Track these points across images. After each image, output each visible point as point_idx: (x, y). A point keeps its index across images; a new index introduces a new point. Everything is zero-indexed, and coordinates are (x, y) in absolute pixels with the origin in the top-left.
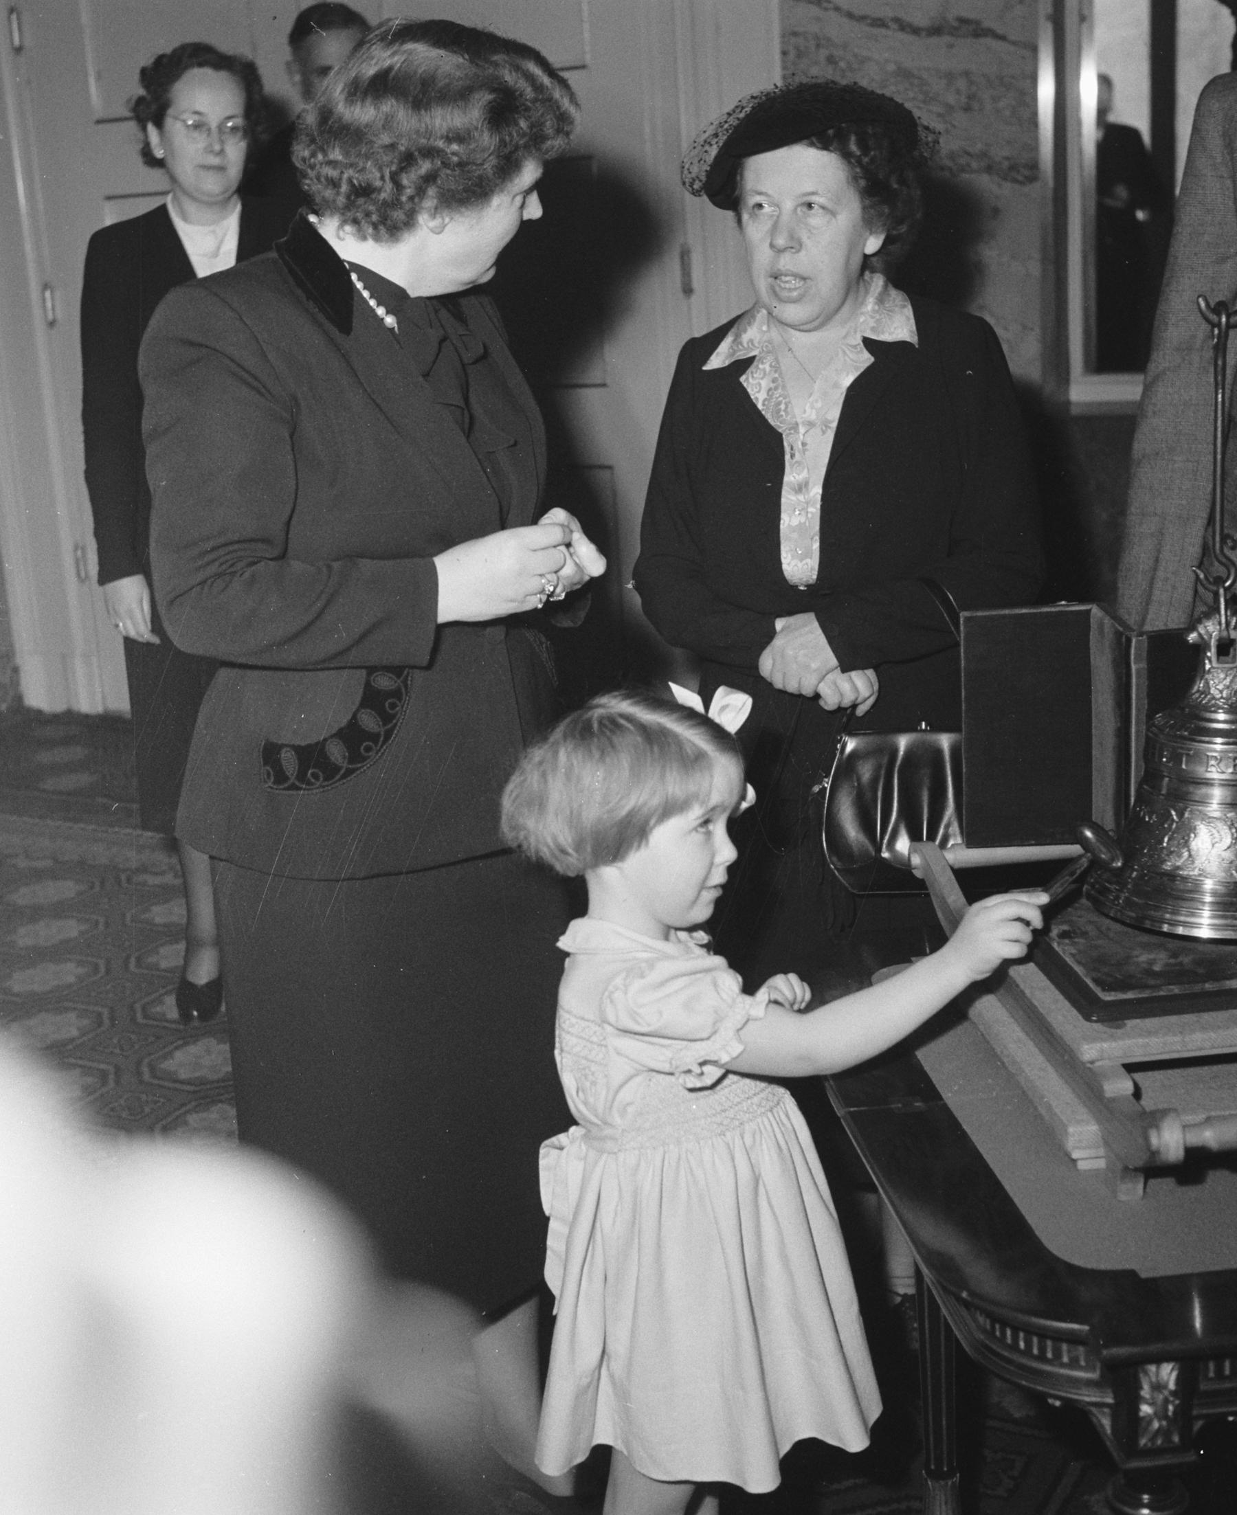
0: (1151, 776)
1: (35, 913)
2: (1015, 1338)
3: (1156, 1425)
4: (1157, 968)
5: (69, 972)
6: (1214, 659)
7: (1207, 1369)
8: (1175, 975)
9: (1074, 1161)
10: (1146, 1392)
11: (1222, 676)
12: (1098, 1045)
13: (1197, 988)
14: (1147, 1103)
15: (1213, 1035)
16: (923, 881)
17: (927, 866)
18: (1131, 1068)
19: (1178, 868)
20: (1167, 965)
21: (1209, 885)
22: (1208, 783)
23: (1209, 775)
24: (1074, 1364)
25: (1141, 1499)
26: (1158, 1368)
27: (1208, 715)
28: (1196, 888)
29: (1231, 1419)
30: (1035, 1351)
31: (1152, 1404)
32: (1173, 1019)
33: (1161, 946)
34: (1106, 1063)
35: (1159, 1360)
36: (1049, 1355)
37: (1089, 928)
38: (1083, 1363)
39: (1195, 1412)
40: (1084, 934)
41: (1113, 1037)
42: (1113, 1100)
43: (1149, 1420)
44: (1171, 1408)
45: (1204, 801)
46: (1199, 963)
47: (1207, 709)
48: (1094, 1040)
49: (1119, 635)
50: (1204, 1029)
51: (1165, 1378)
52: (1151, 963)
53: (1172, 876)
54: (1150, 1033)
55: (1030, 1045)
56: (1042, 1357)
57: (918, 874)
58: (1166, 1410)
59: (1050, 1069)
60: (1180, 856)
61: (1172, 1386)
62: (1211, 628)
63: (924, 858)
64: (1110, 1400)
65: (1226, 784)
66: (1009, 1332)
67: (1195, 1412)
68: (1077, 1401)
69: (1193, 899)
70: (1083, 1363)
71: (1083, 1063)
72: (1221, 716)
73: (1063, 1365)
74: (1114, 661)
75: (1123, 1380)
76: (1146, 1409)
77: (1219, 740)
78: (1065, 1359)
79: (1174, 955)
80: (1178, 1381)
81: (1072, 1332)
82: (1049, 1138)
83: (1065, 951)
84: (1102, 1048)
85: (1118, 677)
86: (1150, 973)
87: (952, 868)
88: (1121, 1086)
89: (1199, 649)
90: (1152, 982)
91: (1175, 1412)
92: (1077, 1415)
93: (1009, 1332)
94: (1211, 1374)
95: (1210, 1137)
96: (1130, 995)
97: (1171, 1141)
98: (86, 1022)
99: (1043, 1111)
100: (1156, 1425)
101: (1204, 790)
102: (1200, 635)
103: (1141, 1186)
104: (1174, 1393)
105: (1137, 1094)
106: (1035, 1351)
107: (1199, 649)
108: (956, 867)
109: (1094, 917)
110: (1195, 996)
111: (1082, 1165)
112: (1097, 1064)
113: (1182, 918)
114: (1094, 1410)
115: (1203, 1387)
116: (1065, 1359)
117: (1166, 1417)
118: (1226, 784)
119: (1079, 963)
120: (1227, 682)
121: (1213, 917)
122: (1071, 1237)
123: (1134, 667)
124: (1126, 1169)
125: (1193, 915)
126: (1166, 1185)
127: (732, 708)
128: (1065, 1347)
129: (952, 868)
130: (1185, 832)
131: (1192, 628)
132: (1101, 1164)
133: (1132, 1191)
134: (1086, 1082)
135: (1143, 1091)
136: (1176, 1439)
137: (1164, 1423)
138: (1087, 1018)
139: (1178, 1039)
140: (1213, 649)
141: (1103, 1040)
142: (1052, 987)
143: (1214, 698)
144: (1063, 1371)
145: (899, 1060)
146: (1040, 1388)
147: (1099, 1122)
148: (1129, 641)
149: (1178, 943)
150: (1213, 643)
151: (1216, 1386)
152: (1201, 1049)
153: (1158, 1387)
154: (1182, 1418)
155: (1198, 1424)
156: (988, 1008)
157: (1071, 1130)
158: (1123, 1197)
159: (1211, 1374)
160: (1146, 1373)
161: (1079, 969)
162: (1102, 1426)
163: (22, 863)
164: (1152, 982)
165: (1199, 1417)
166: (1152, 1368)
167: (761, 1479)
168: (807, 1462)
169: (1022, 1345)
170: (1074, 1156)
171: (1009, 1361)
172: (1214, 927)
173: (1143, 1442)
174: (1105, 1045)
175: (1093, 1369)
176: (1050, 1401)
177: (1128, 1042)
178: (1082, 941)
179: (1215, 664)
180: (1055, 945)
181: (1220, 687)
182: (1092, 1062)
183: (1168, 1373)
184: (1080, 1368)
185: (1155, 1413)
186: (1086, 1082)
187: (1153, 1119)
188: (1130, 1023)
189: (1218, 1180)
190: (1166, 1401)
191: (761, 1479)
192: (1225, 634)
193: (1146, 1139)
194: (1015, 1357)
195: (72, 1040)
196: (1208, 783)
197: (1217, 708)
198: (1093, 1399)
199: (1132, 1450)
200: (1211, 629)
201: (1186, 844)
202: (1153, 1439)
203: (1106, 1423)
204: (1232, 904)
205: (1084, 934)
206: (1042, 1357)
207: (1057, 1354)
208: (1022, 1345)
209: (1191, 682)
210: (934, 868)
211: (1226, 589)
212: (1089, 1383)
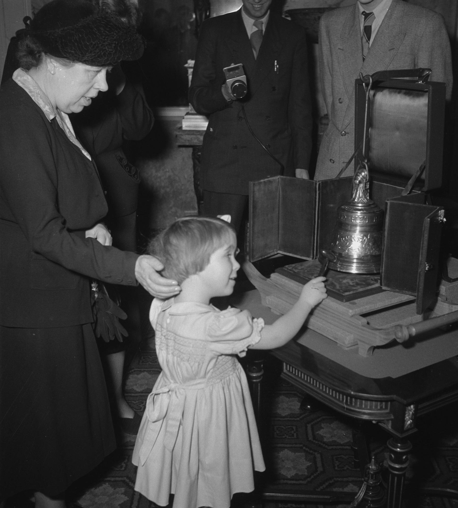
22: (356, 226)
118: (361, 226)
176: (208, 11)
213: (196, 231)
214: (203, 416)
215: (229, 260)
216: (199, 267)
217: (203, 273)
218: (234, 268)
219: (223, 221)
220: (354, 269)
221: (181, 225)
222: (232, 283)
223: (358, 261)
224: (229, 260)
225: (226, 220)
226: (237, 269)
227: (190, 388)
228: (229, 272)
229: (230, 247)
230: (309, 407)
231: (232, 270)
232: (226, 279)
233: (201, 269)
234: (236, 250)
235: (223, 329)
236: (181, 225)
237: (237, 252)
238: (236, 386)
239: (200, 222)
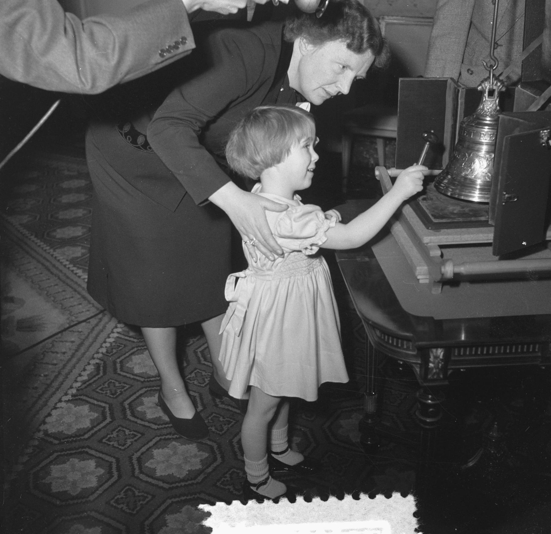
0: (462, 140)
1: (69, 191)
2: (388, 339)
3: (434, 371)
4: (455, 212)
5: (65, 199)
6: (487, 97)
7: (455, 352)
8: (462, 214)
9: (418, 280)
10: (432, 359)
11: (489, 103)
12: (430, 238)
13: (469, 219)
14: (445, 257)
15: (472, 236)
16: (379, 181)
17: (381, 175)
18: (441, 247)
19: (467, 175)
20: (459, 211)
21: (479, 182)
22: (481, 144)
23: (481, 141)
24: (408, 349)
25: (428, 397)
26: (437, 350)
27: (483, 118)
28: (481, 190)
29: (462, 370)
30: (395, 344)
31: (433, 363)
32: (459, 230)
33: (458, 205)
34: (432, 244)
35: (437, 347)
36: (400, 345)
37: (434, 198)
38: (411, 348)
39: (449, 367)
40: (432, 199)
41: (435, 235)
42: (433, 257)
43: (432, 369)
44: (440, 365)
45: (479, 150)
46: (471, 211)
47: (482, 115)
48: (428, 236)
49: (455, 88)
50: (469, 233)
51: (439, 354)
52: (454, 210)
53: (465, 178)
54: (448, 234)
55: (409, 239)
56: (397, 346)
57: (378, 178)
58: (438, 365)
59: (414, 247)
60: (468, 170)
61: (441, 357)
62: (486, 85)
63: (380, 172)
64: (419, 362)
65: (487, 144)
66: (386, 337)
67: (449, 367)
68: (408, 362)
69: (471, 187)
70: (411, 348)
71: (424, 244)
72: (488, 119)
73: (404, 349)
74: (453, 98)
75: (424, 353)
76: (431, 365)
77: (487, 127)
78: (405, 347)
79: (463, 208)
80: (444, 356)
81: (406, 336)
82: (411, 271)
83: (424, 205)
84: (433, 239)
85: (454, 105)
86: (453, 213)
87: (390, 177)
88: (438, 252)
89: (482, 93)
90: (452, 216)
91: (442, 367)
92: (408, 367)
93: (386, 337)
94: (456, 354)
95: (463, 270)
96: (444, 221)
97: (449, 270)
98: (85, 230)
99: (409, 262)
100: (434, 371)
101: (481, 146)
102: (483, 87)
103: (440, 289)
104: (442, 360)
105: (442, 256)
106: (395, 344)
107: (482, 93)
108: (392, 176)
109: (437, 194)
110: (467, 222)
111: (421, 281)
112: (429, 244)
113: (464, 193)
114: (414, 365)
115: (453, 358)
116: (405, 347)
117: (438, 368)
118: (487, 144)
119: (427, 209)
120: (491, 106)
121: (479, 194)
122: (410, 304)
123: (459, 101)
124: (435, 281)
125: (470, 192)
126: (447, 287)
127: (306, 106)
128: (405, 342)
129: (390, 177)
130: (472, 161)
131: (480, 85)
132: (427, 281)
133: (437, 291)
134: (423, 249)
135: (444, 254)
136: (441, 376)
137: (437, 370)
138: (428, 228)
139: (459, 236)
140: (487, 93)
141: (431, 236)
142: (417, 217)
143: (485, 112)
144: (404, 351)
145: (366, 248)
146: (395, 357)
147: (428, 266)
148: (459, 91)
149: (465, 204)
150: (487, 90)
151: (457, 358)
152: (467, 241)
153: (436, 357)
154: (444, 369)
155: (450, 372)
156: (398, 228)
157: (418, 268)
158: (433, 292)
159: (456, 354)
160: (432, 352)
161: (427, 211)
162: (416, 371)
163: (66, 173)
164: (452, 216)
165: (450, 369)
166: (434, 350)
167: (311, 396)
168: (326, 390)
169: (390, 341)
170: (418, 277)
171: (386, 347)
172: (479, 197)
173: (429, 377)
174: (432, 237)
175: (414, 351)
176: (399, 362)
177: (441, 237)
178: (430, 201)
179: (487, 99)
180: (420, 203)
181: (488, 108)
182: (427, 244)
183: (440, 353)
184: (410, 350)
185: (434, 367)
186: (423, 249)
187: (443, 263)
188: (442, 231)
189: (465, 287)
190: (439, 363)
191: (311, 396)
192: (491, 87)
193: (440, 269)
194: (388, 346)
195: (79, 236)
196: (481, 144)
197: (487, 116)
198: (414, 361)
199: (425, 379)
200: (487, 86)
201: (470, 167)
202: (433, 376)
203: (418, 370)
204: (485, 189)
205: (432, 199)
206: (397, 346)
207: (402, 345)
208: (390, 341)
209: (478, 105)
210: (383, 175)
211: (493, 70)
212: (413, 356)
213: (274, 121)
214: (264, 309)
215: (308, 151)
216: (277, 159)
217: (281, 165)
218: (313, 159)
219: (301, 110)
220: (476, 197)
221: (259, 114)
222: (310, 175)
223: (480, 195)
224: (308, 151)
225: (304, 108)
226: (316, 161)
227: (260, 277)
228: (307, 164)
229: (308, 139)
230: (524, 243)
231: (311, 161)
232: (306, 170)
233: (279, 162)
234: (316, 140)
235: (236, 136)
236: (259, 114)
237: (317, 142)
238: (308, 288)
239: (278, 111)
